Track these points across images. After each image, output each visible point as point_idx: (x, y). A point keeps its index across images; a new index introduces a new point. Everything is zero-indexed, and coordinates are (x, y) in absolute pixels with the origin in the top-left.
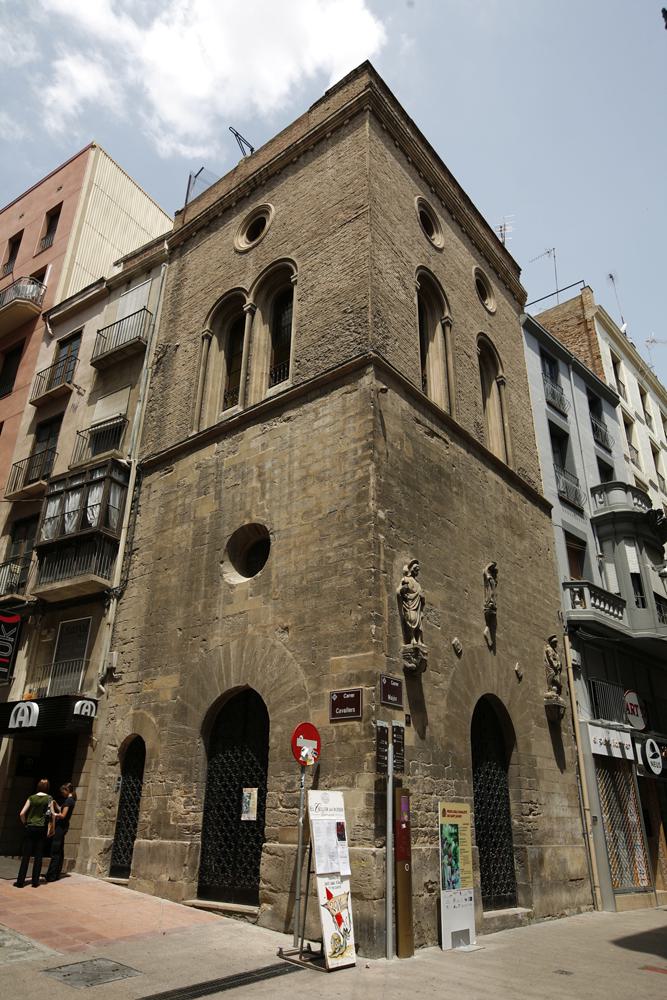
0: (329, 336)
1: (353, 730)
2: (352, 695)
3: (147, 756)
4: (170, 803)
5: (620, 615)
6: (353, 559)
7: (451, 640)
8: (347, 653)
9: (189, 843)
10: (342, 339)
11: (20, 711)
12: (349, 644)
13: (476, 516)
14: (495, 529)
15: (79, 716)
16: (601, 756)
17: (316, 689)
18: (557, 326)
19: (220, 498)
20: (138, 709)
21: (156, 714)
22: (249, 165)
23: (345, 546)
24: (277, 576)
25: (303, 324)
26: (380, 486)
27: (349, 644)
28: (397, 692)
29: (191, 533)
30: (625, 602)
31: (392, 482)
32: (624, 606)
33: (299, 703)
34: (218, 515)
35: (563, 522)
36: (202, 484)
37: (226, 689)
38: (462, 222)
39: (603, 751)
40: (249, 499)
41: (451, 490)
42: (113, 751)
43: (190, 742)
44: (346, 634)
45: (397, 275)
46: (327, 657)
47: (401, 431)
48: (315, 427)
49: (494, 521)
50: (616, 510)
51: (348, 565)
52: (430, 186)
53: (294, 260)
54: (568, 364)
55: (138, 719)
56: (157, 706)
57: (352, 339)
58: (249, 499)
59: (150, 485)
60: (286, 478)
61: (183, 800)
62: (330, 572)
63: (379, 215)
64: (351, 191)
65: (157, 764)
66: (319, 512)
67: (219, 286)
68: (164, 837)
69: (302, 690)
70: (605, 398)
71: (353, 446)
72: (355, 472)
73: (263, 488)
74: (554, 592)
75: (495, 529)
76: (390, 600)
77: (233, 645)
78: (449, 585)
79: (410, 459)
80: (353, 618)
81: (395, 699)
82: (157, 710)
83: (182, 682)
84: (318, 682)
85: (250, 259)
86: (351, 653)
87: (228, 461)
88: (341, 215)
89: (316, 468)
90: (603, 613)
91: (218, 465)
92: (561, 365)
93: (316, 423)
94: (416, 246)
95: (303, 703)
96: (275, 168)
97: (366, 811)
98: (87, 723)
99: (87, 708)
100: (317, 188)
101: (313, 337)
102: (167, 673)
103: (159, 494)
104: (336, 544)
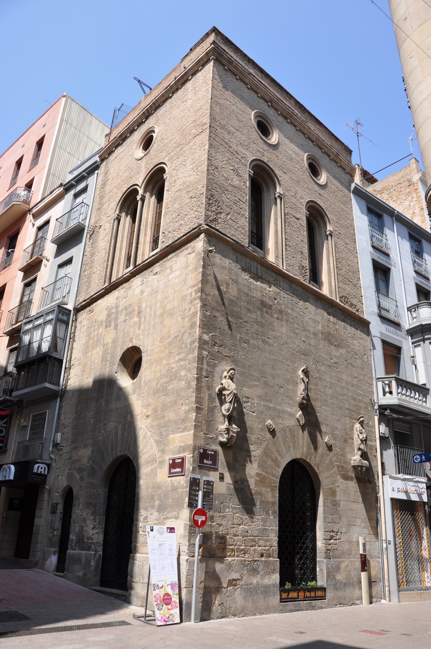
0: (181, 215)
1: (179, 483)
2: (180, 460)
3: (74, 499)
4: (85, 528)
5: (424, 399)
6: (185, 369)
7: (265, 422)
8: (178, 432)
9: (93, 553)
10: (189, 216)
11: (5, 469)
12: (181, 426)
13: (294, 333)
14: (312, 342)
15: (37, 474)
16: (404, 500)
17: (161, 457)
18: (394, 188)
19: (117, 329)
20: (71, 469)
21: (79, 473)
22: (146, 100)
23: (182, 360)
24: (144, 382)
25: (168, 207)
26: (206, 317)
27: (181, 426)
28: (214, 457)
29: (101, 353)
30: (428, 390)
31: (217, 314)
32: (428, 393)
33: (152, 465)
34: (115, 341)
35: (381, 333)
36: (108, 320)
37: (115, 456)
38: (297, 124)
39: (403, 497)
40: (132, 330)
41: (272, 316)
42: (57, 496)
43: (95, 490)
44: (179, 419)
45: (232, 168)
46: (168, 435)
47: (227, 278)
48: (170, 278)
49: (312, 336)
50: (423, 323)
51: (183, 373)
52: (267, 102)
53: (166, 163)
54: (392, 217)
55: (70, 477)
56: (80, 468)
57: (194, 216)
58: (132, 330)
59: (81, 321)
60: (153, 314)
61: (91, 526)
62: (173, 378)
63: (218, 129)
64: (200, 114)
65: (79, 505)
66: (169, 337)
67: (125, 184)
68: (82, 549)
69: (154, 458)
70: (424, 239)
71: (190, 291)
72: (190, 309)
73: (140, 321)
74: (368, 385)
75: (312, 342)
76: (210, 395)
77: (120, 427)
78: (266, 384)
79: (234, 296)
80: (184, 409)
81: (210, 462)
82: (80, 470)
83: (93, 453)
84: (163, 452)
85: (143, 163)
86: (182, 432)
87: (123, 303)
88: (194, 131)
89: (169, 307)
90: (408, 398)
91: (117, 307)
92: (387, 218)
93: (171, 276)
94: (252, 145)
95: (154, 466)
96: (159, 102)
97: (184, 534)
98: (43, 478)
99: (42, 468)
100: (182, 113)
101: (173, 216)
102: (85, 446)
103: (85, 328)
104: (177, 359)
